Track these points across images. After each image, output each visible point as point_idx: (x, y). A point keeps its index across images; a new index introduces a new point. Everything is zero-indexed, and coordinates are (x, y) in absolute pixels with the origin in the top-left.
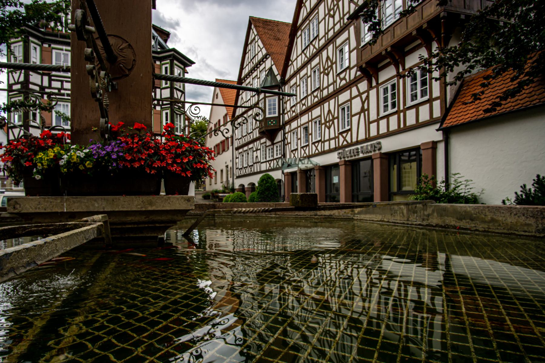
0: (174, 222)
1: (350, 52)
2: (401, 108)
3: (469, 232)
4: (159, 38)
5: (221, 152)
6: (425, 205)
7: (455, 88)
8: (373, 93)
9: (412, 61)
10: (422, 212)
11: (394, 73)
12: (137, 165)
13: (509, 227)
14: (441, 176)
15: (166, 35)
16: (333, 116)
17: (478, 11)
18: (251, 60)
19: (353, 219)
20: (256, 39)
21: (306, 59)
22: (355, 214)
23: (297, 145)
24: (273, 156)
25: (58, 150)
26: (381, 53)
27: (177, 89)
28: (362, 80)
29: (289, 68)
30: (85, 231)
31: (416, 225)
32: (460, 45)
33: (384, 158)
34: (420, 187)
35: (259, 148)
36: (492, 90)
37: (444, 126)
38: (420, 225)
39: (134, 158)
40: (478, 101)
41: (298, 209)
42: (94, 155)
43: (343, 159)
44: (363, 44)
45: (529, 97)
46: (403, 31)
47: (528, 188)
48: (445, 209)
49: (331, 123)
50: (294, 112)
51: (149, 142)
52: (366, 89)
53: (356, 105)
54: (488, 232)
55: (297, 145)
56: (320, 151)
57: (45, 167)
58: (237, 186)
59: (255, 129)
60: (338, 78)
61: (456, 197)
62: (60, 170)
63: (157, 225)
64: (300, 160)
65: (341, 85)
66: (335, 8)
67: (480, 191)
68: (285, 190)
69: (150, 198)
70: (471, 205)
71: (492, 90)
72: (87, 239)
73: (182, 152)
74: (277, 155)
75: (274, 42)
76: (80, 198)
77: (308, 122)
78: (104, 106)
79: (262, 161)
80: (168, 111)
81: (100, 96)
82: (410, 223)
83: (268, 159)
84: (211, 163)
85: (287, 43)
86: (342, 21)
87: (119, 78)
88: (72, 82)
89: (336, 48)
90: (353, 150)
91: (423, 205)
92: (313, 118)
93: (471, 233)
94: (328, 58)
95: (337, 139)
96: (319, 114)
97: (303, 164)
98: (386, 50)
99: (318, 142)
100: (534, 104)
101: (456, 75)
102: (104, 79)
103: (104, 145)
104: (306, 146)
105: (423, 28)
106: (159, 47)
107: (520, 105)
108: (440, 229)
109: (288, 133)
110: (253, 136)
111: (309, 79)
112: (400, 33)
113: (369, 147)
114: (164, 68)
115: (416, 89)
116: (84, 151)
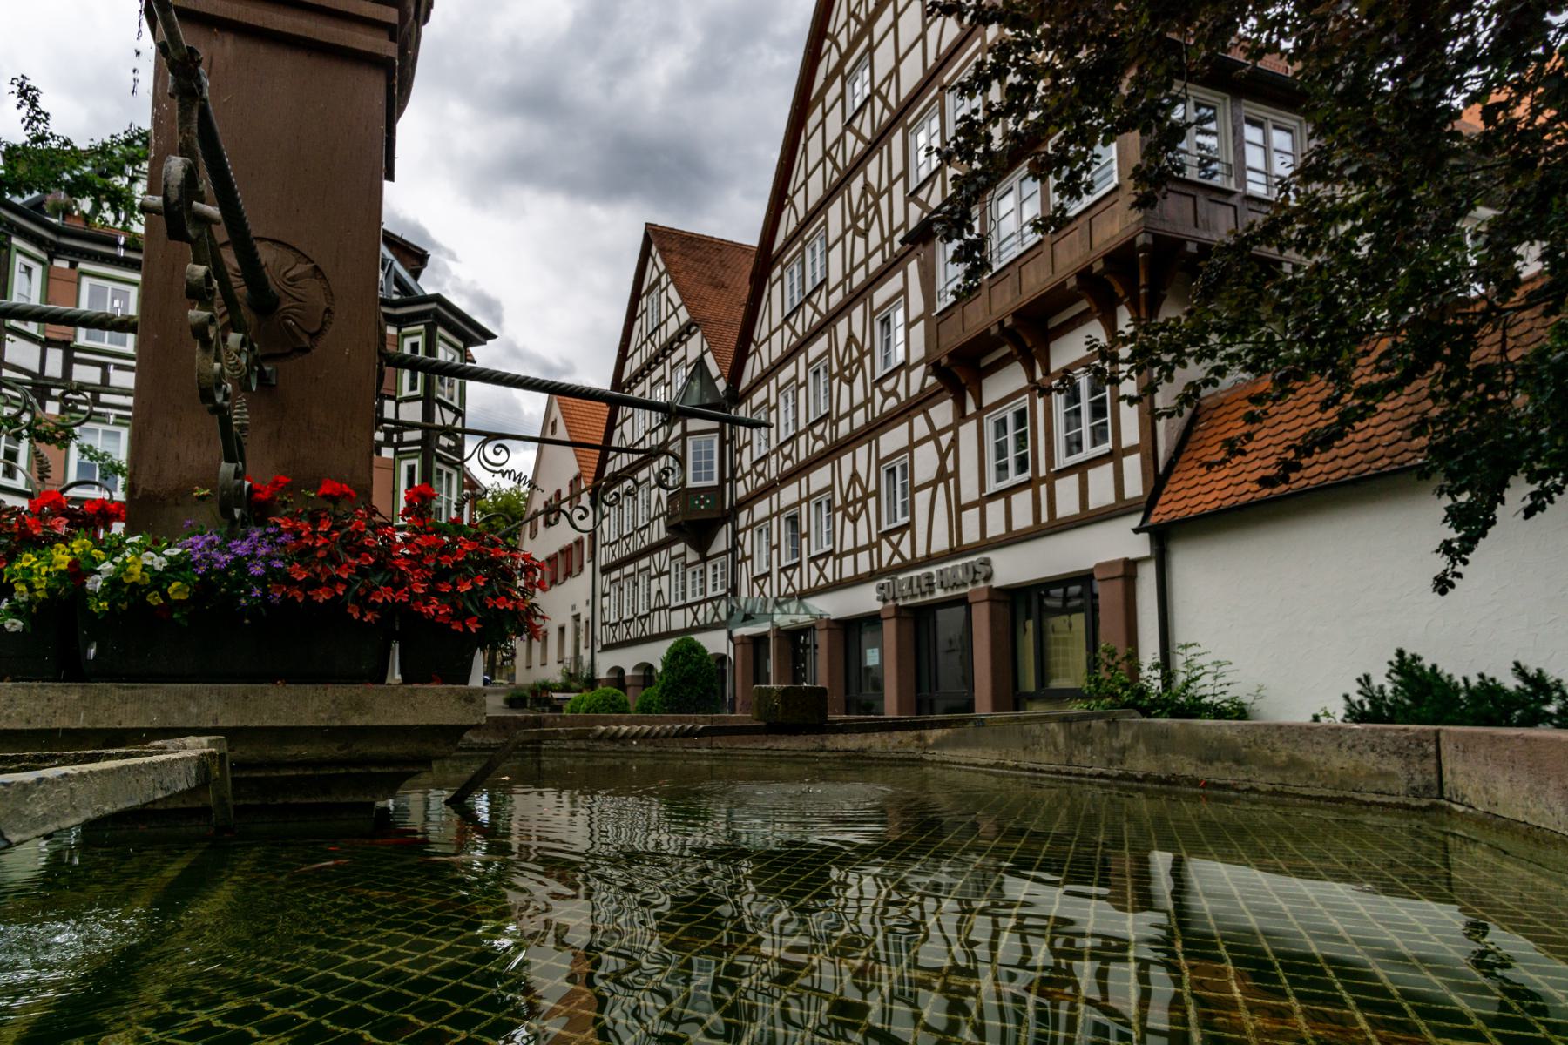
0: (425, 762)
1: (909, 325)
2: (1042, 473)
3: (1233, 794)
4: (397, 265)
5: (560, 580)
6: (1113, 722)
7: (1179, 422)
8: (968, 431)
9: (1069, 351)
10: (1106, 741)
11: (1022, 381)
12: (322, 596)
13: (1337, 782)
14: (1149, 651)
15: (415, 258)
16: (864, 490)
17: (1231, 232)
18: (649, 337)
19: (921, 759)
20: (664, 284)
21: (794, 339)
22: (927, 747)
23: (770, 563)
24: (703, 591)
25: (83, 546)
26: (988, 330)
27: (443, 404)
28: (939, 397)
29: (749, 362)
30: (163, 763)
31: (1090, 776)
32: (1190, 313)
33: (999, 601)
34: (1096, 680)
35: (666, 568)
36: (1272, 432)
37: (1153, 520)
38: (1101, 775)
39: (317, 575)
40: (1239, 458)
41: (775, 728)
42: (195, 564)
43: (891, 603)
44: (940, 306)
45: (1366, 452)
46: (1043, 276)
47: (1375, 683)
48: (1165, 734)
49: (859, 506)
50: (760, 475)
51: (361, 535)
52: (950, 421)
53: (926, 462)
54: (1282, 794)
55: (770, 563)
56: (831, 580)
57: (39, 594)
58: (602, 673)
59: (655, 518)
60: (877, 391)
61: (1192, 706)
62: (85, 605)
63: (374, 770)
64: (777, 604)
65: (885, 409)
66: (871, 213)
67: (1253, 690)
68: (735, 685)
69: (357, 690)
70: (1234, 722)
71: (1272, 432)
72: (167, 790)
73: (456, 563)
74: (714, 590)
75: (708, 292)
76: (141, 689)
77: (798, 504)
78: (235, 429)
79: (673, 604)
80: (416, 462)
81: (225, 399)
82: (1075, 770)
83: (690, 599)
84: (539, 597)
85: (744, 297)
86: (887, 245)
87: (285, 356)
88: (140, 372)
89: (873, 314)
90: (918, 577)
91: (1109, 723)
92: (812, 492)
93: (1238, 798)
94: (851, 338)
95: (875, 550)
96: (829, 482)
97: (784, 613)
98: (1001, 323)
99: (826, 555)
100: (1379, 469)
101: (1180, 391)
102: (239, 353)
103: (231, 535)
104: (793, 567)
105: (1094, 271)
106: (395, 288)
107: (1344, 471)
108: (1157, 786)
109: (744, 530)
110: (650, 537)
111: (802, 391)
112: (1036, 281)
113: (960, 573)
114: (411, 341)
115: (1079, 425)
116: (167, 552)
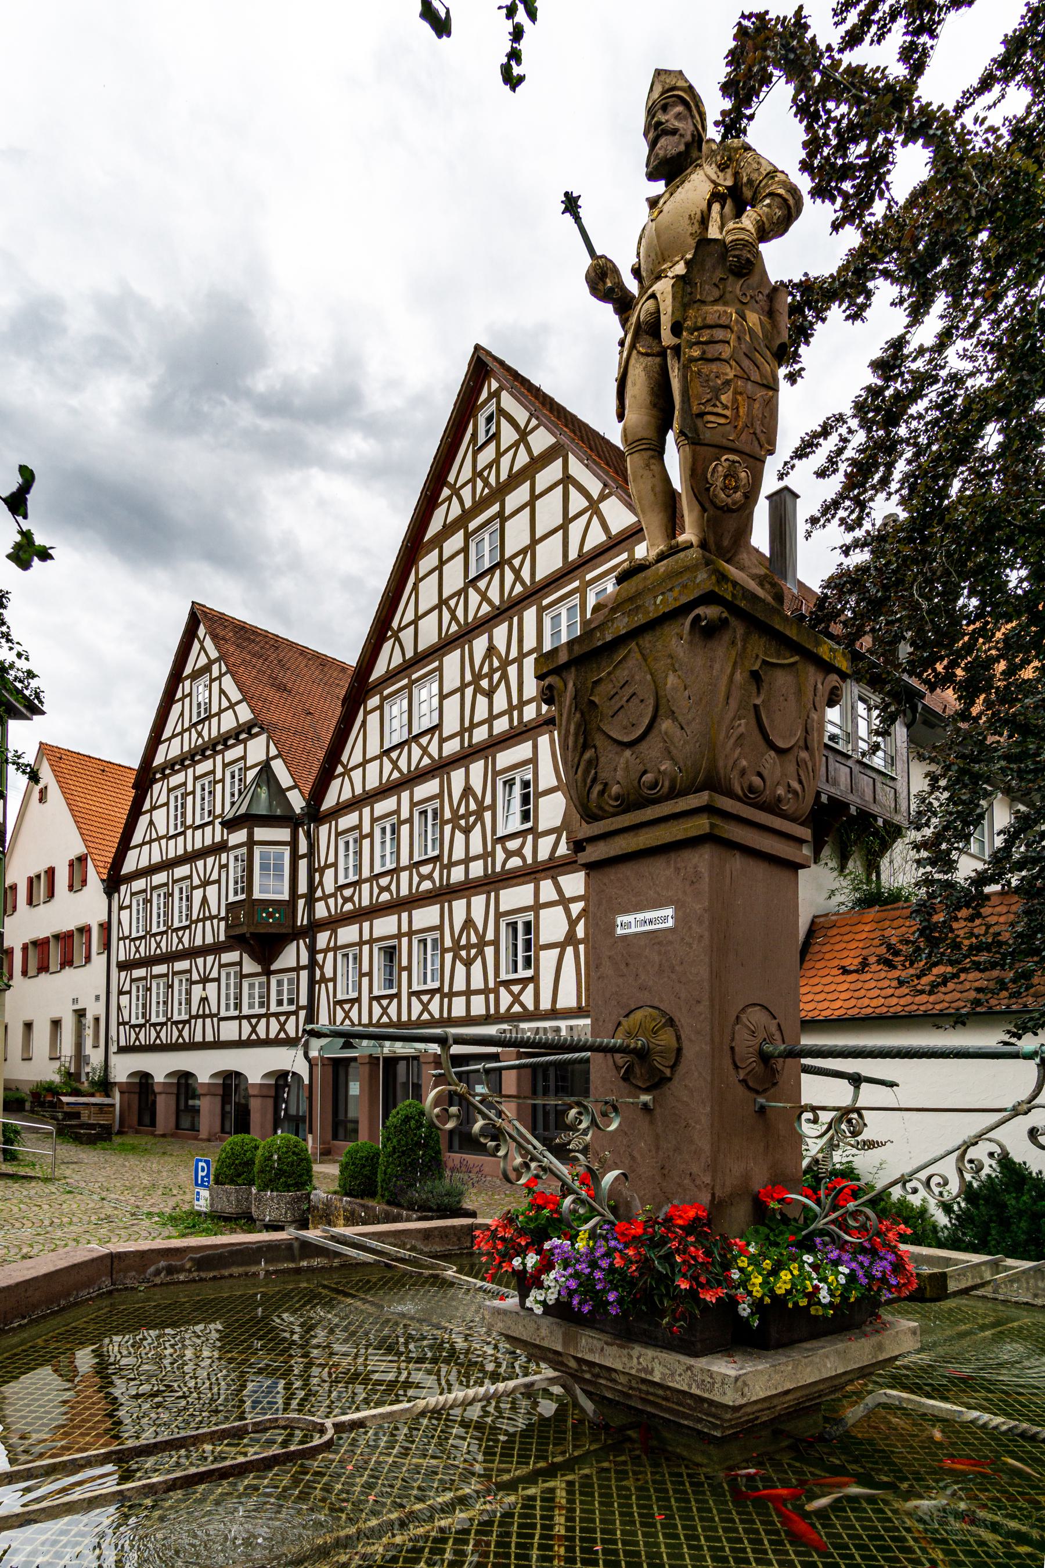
16: (480, 803)
29: (335, 784)
77: (399, 936)
99: (432, 992)
109: (325, 951)
